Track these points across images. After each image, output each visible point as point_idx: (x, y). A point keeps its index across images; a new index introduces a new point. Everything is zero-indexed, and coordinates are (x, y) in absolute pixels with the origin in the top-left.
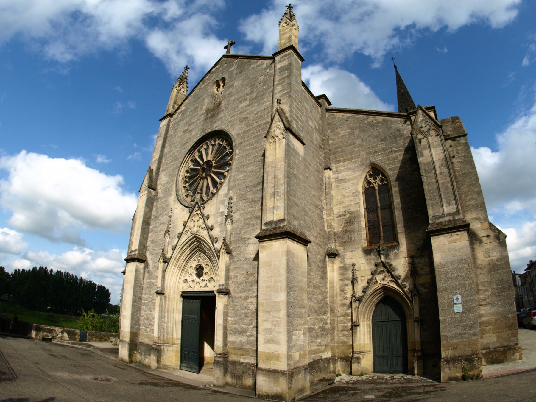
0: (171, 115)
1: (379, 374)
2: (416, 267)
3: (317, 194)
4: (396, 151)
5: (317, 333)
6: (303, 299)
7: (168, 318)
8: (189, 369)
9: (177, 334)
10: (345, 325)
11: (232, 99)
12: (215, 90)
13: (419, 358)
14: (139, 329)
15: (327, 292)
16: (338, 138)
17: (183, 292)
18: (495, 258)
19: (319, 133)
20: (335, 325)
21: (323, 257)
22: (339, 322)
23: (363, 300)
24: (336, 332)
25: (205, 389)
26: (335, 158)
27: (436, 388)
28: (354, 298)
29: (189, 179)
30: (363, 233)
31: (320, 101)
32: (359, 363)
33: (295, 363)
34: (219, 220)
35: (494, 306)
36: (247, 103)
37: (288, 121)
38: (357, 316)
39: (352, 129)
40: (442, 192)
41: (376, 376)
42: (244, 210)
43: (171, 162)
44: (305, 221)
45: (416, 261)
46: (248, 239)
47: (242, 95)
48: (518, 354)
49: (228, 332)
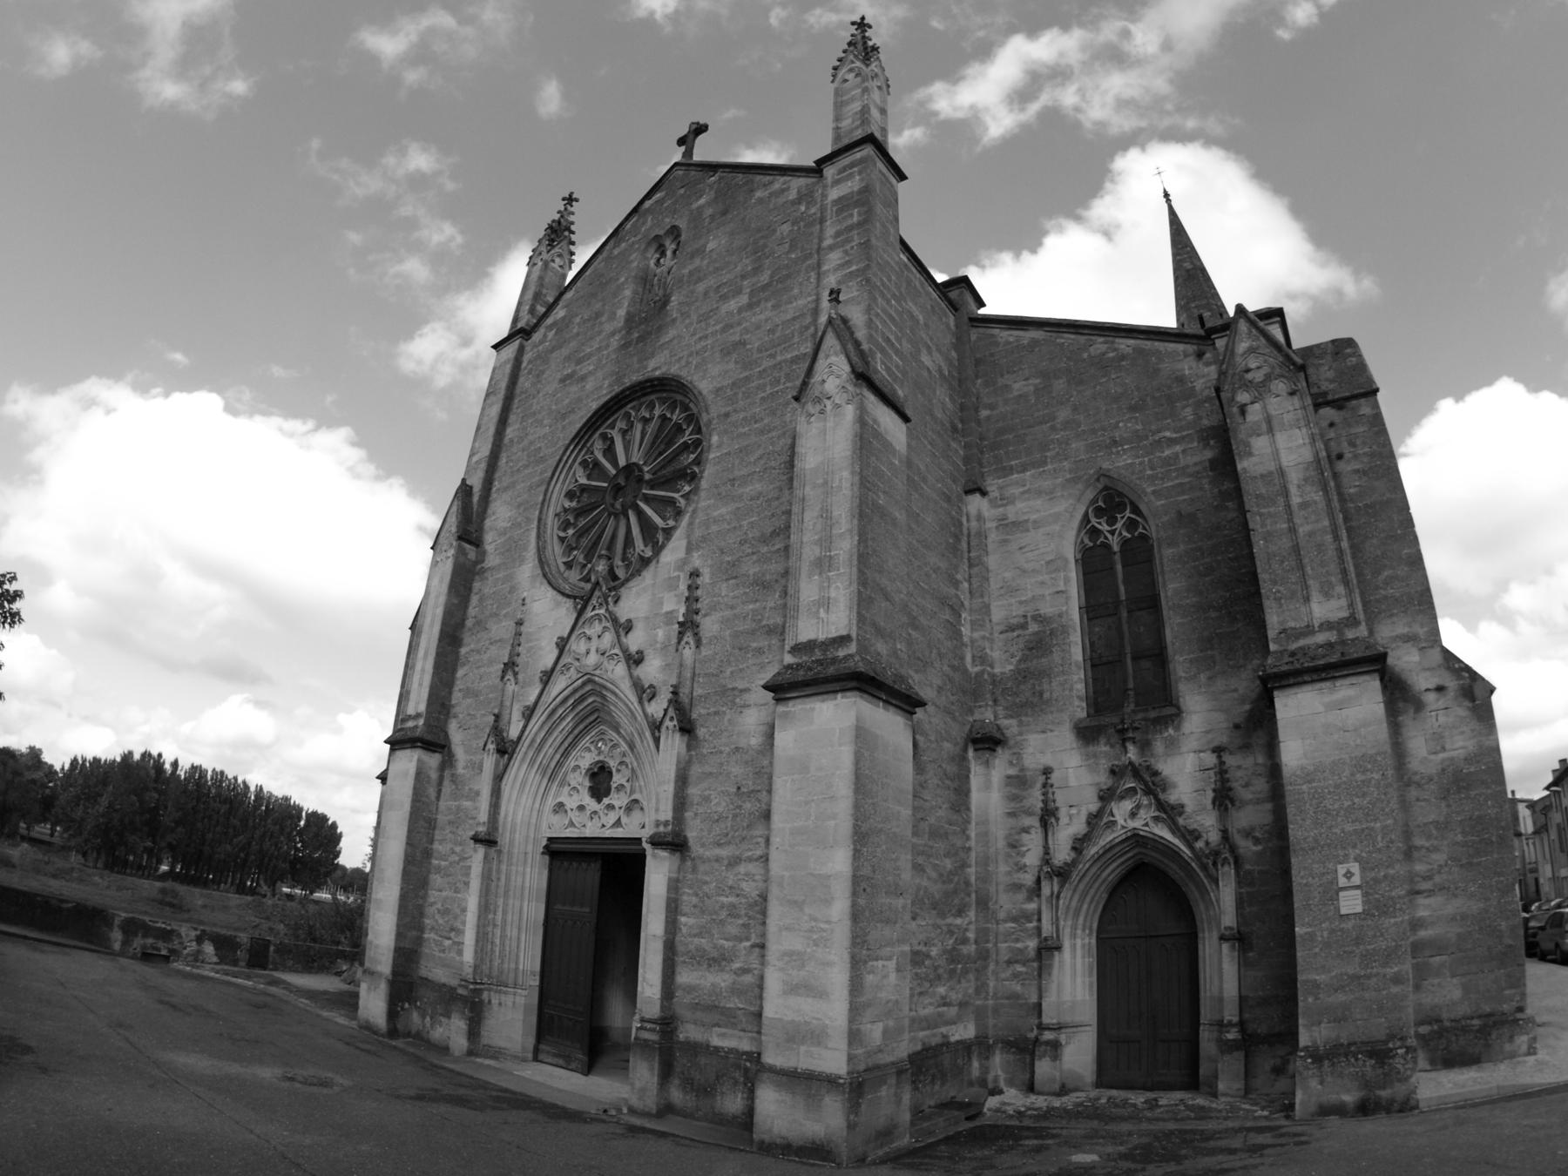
1: (1114, 1093)
2: (1228, 780)
3: (943, 565)
4: (1172, 442)
5: (936, 968)
7: (505, 913)
8: (561, 1062)
9: (529, 957)
10: (1019, 945)
11: (701, 287)
12: (652, 262)
14: (419, 941)
15: (969, 849)
17: (550, 839)
18: (1461, 753)
20: (990, 945)
22: (1001, 938)
24: (992, 967)
25: (604, 1121)
27: (1282, 1135)
28: (1046, 869)
29: (576, 518)
31: (953, 295)
33: (869, 1054)
34: (660, 633)
35: (1455, 896)
36: (744, 299)
37: (862, 354)
38: (1056, 922)
40: (1306, 561)
41: (1105, 1095)
42: (732, 608)
43: (526, 467)
48: (1525, 1038)
49: (679, 959)
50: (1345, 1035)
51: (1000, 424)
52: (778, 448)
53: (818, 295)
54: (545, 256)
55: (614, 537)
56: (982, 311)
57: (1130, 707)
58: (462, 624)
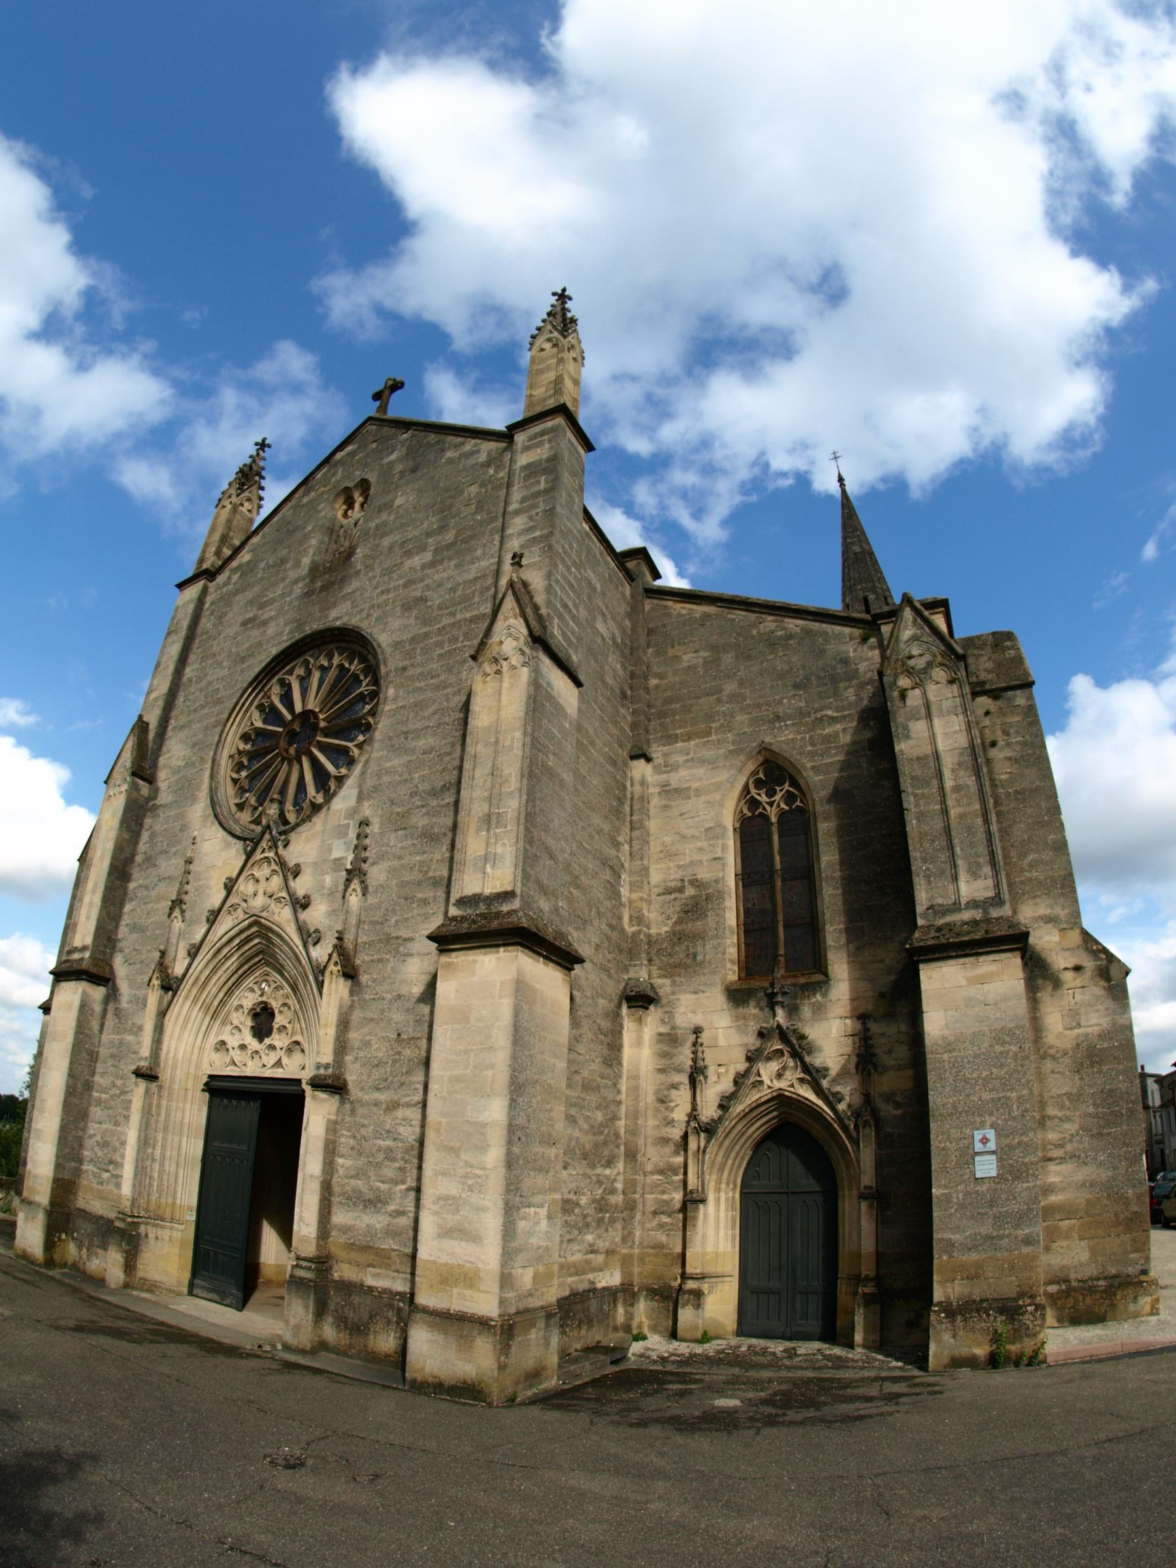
0: (209, 574)
1: (754, 1341)
2: (872, 1046)
5: (585, 1216)
6: (551, 1119)
7: (164, 1147)
8: (215, 1297)
9: (187, 1194)
10: (665, 1197)
11: (386, 542)
12: (340, 513)
13: (869, 1300)
14: (78, 1172)
15: (620, 1102)
16: (675, 672)
17: (210, 1076)
18: (1095, 1030)
19: (623, 656)
20: (637, 1196)
21: (613, 1005)
22: (648, 1189)
23: (720, 1130)
24: (638, 1217)
25: (259, 1357)
26: (664, 727)
27: (916, 1385)
28: (693, 1124)
29: (250, 760)
30: (728, 942)
31: (631, 565)
32: (698, 1306)
33: (520, 1298)
34: (328, 879)
35: (1085, 1164)
36: (428, 556)
37: (540, 618)
38: (701, 1175)
39: (714, 649)
40: (956, 841)
41: (745, 1343)
42: (400, 858)
43: (203, 707)
44: (570, 900)
45: (874, 1028)
46: (405, 940)
47: (415, 533)
48: (1148, 1299)
49: (335, 1200)
50: (977, 1292)
51: (669, 694)
52: (452, 704)
53: (500, 557)
54: (234, 499)
55: (286, 782)
56: (658, 583)
57: (780, 972)
58: (131, 859)
